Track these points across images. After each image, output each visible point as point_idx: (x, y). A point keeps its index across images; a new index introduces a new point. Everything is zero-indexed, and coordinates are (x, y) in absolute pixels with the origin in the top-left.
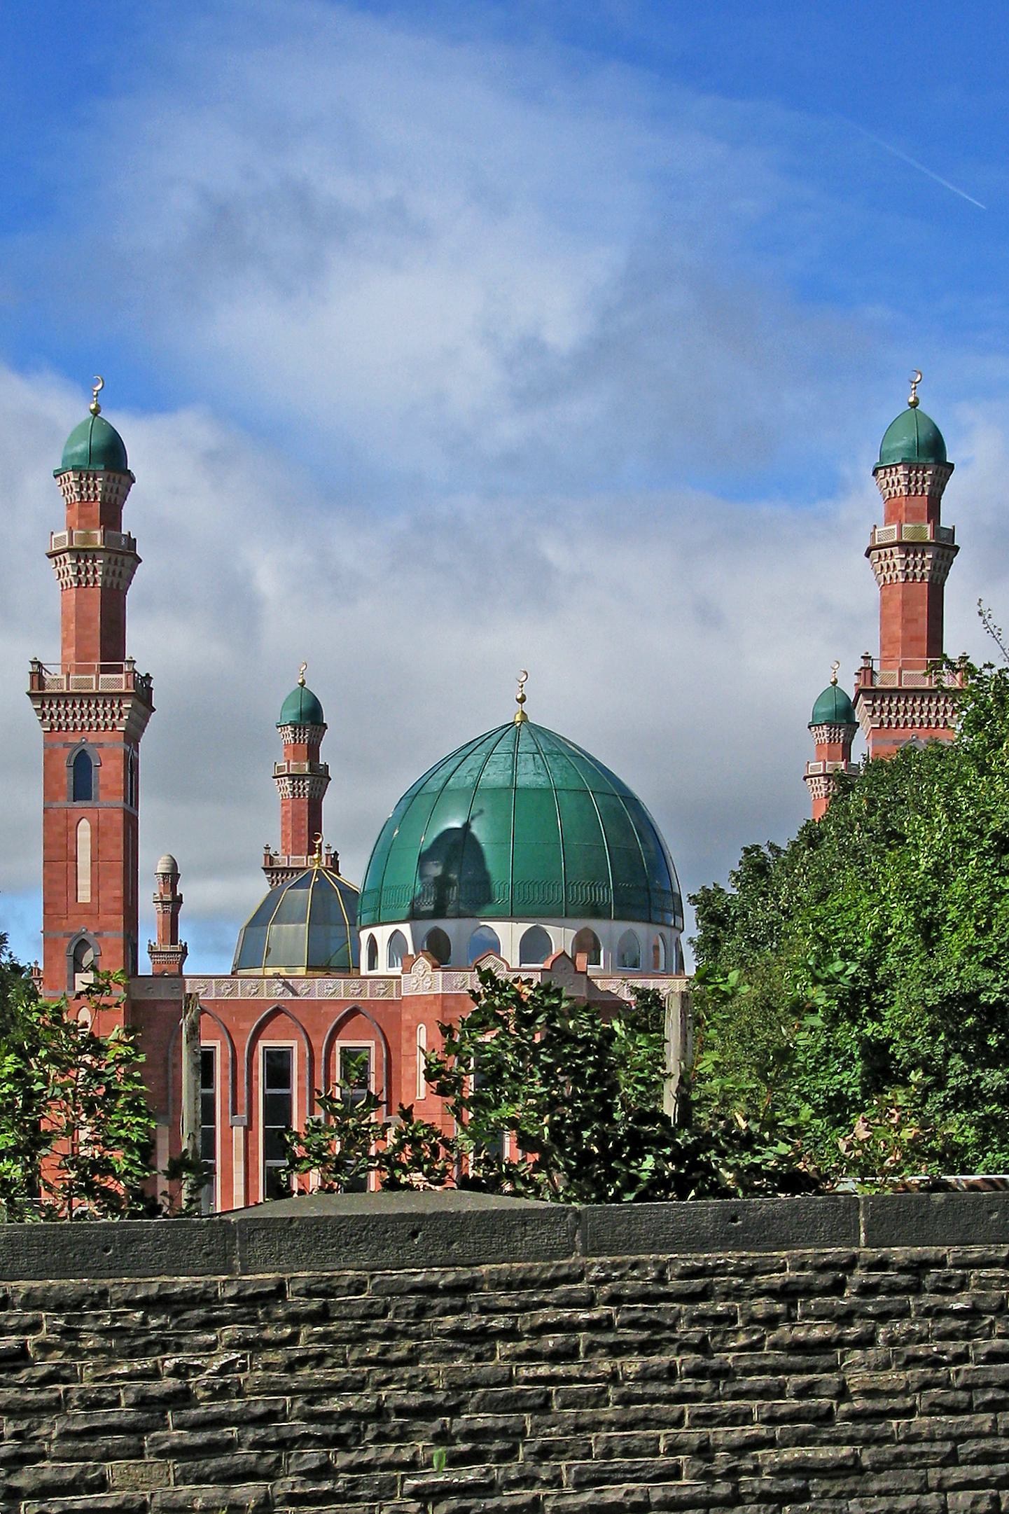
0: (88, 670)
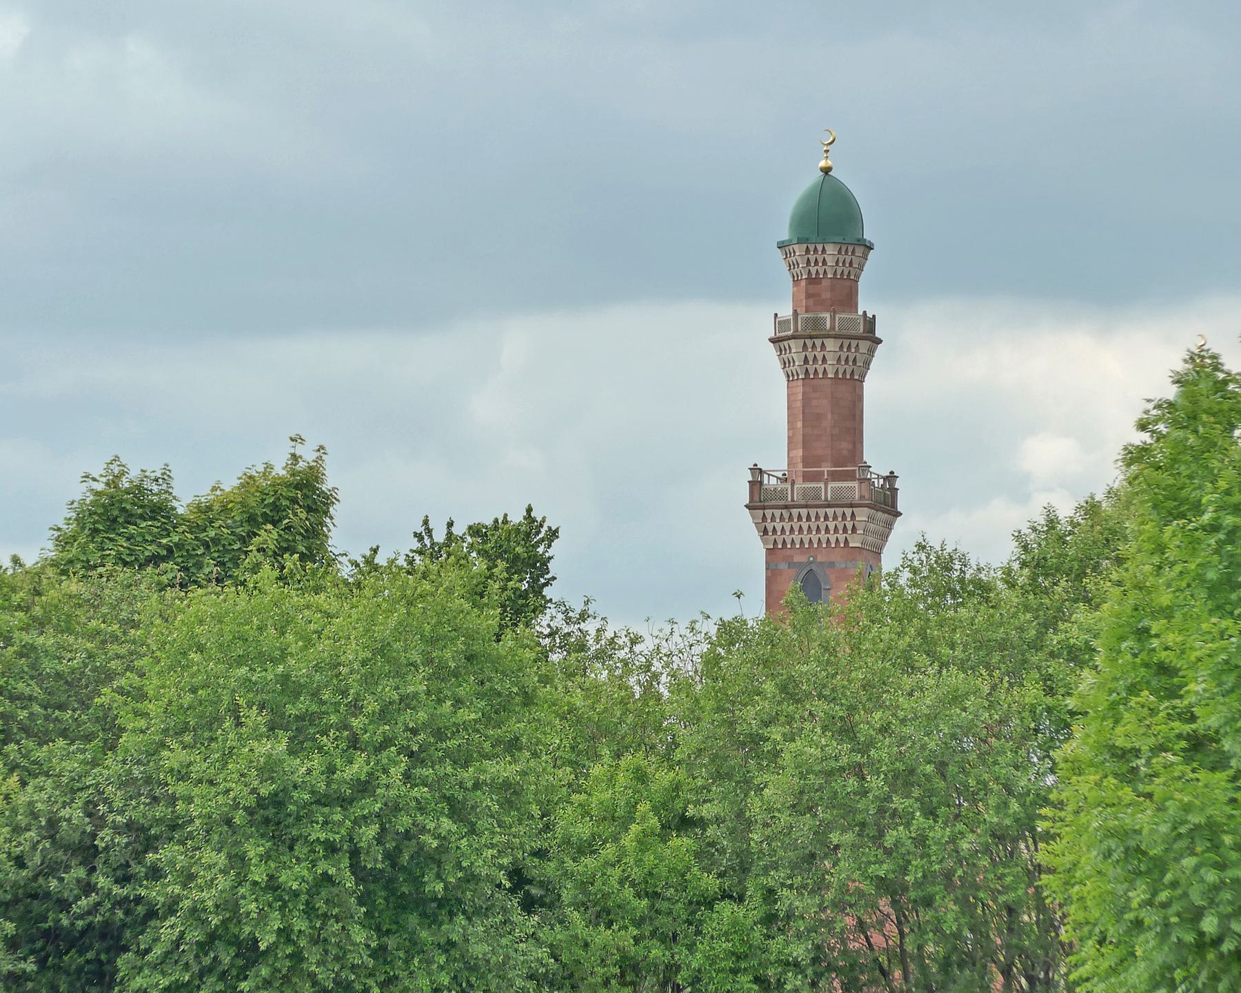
0: (816, 477)
